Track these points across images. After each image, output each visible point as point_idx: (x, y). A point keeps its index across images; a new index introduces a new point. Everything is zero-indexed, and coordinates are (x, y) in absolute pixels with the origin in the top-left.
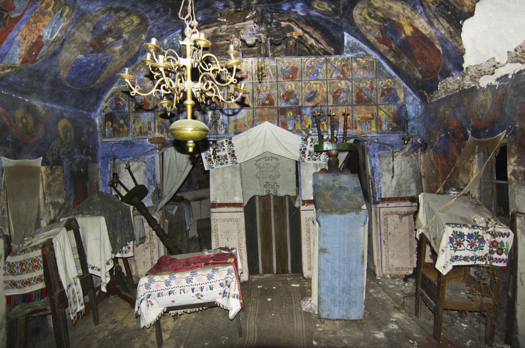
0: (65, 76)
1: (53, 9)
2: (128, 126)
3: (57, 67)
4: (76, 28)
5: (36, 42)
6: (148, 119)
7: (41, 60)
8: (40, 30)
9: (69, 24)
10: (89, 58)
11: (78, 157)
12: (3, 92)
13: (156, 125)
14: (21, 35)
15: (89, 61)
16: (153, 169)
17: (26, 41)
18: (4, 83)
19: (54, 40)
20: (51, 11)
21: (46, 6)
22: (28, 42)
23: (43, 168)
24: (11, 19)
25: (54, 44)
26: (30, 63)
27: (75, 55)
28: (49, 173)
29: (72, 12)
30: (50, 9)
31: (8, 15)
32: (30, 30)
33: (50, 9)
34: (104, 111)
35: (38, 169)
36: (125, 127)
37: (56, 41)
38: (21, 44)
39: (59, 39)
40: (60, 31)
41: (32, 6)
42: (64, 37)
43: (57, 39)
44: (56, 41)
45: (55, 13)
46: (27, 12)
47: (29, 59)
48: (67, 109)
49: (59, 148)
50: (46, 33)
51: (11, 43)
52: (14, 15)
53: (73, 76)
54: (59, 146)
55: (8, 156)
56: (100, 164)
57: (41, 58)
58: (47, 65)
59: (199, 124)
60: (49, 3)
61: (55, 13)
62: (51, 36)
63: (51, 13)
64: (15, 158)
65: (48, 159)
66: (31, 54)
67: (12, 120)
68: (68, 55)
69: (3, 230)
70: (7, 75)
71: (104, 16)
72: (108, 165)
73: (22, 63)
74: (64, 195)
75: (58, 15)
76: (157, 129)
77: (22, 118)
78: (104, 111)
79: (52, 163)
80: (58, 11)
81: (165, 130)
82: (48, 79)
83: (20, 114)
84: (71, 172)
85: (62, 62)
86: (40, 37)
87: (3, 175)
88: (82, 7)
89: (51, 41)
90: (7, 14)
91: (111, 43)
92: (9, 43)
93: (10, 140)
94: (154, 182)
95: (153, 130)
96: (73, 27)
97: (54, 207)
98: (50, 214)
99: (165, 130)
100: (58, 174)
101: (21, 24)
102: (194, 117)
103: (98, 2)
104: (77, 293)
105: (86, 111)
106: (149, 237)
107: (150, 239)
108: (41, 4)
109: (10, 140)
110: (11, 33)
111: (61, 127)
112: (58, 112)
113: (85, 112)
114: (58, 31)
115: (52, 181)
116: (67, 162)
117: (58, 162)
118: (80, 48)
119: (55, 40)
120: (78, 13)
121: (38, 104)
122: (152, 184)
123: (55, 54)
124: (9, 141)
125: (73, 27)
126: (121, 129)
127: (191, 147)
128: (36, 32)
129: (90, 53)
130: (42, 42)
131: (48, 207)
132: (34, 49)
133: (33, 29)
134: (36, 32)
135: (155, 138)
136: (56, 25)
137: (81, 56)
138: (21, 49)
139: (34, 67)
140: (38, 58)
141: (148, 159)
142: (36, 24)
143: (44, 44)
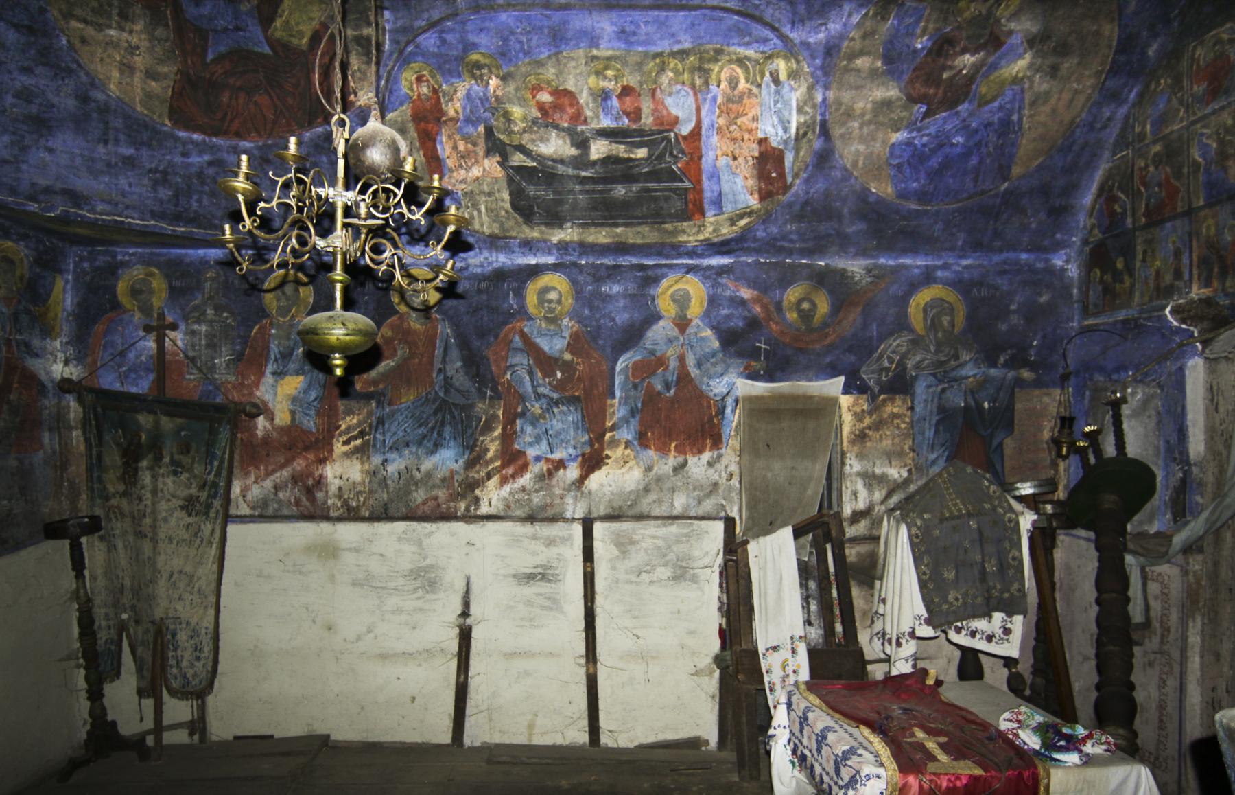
0: (889, 190)
1: (747, 81)
2: (1131, 275)
3: (852, 181)
4: (834, 85)
5: (761, 153)
6: (1174, 243)
7: (798, 181)
8: (752, 130)
9: (810, 89)
10: (932, 130)
11: (972, 373)
12: (762, 260)
13: (1195, 258)
14: (723, 155)
15: (937, 136)
16: (1179, 409)
17: (741, 160)
18: (752, 245)
19: (797, 133)
20: (748, 86)
21: (730, 84)
22: (747, 162)
23: (846, 401)
24: (685, 138)
25: (805, 140)
26: (778, 193)
27: (880, 140)
28: (863, 411)
29: (798, 62)
30: (743, 85)
31: (676, 135)
32: (734, 140)
33: (743, 85)
34: (1087, 240)
35: (833, 403)
36: (1126, 277)
37: (805, 134)
38: (734, 170)
39: (808, 127)
40: (800, 110)
41: (705, 100)
42: (819, 118)
43: (805, 129)
44: (805, 134)
45: (759, 86)
46: (703, 113)
47: (771, 188)
48: (951, 261)
49: (904, 357)
50: (771, 130)
51: (715, 176)
52: (685, 130)
53: (915, 185)
54: (904, 349)
55: (753, 376)
56: (1070, 389)
57: (796, 176)
58: (820, 186)
59: (359, 320)
60: (731, 76)
61: (759, 86)
62: (785, 130)
63: (750, 90)
64: (771, 379)
65: (862, 380)
66: (769, 177)
67: (772, 308)
68: (862, 148)
69: (727, 508)
70: (747, 229)
71: (891, 22)
72: (1084, 394)
73: (762, 199)
74: (909, 461)
75: (768, 86)
76: (1195, 272)
77: (800, 301)
78: (1087, 240)
79: (876, 389)
80: (762, 78)
81: (1216, 270)
82: (845, 211)
83: (796, 294)
84: (942, 410)
85: (855, 164)
86: (763, 141)
87: (737, 411)
88: (811, 40)
89: (793, 137)
90: (672, 135)
91: (977, 68)
92: (712, 177)
93: (763, 346)
94: (1181, 453)
95: (1186, 277)
96: (827, 87)
97: (870, 485)
98: (856, 498)
99: (1216, 270)
100: (893, 413)
101: (708, 137)
102: (348, 305)
103: (841, 6)
104: (794, 672)
105: (1028, 251)
106: (1159, 631)
107: (1162, 642)
108: (718, 86)
109: (763, 346)
110: (704, 159)
111: (918, 305)
112: (916, 271)
113: (1024, 256)
114: (794, 112)
115: (869, 428)
116: (928, 387)
117: (899, 385)
118: (881, 118)
119: (801, 132)
120: (813, 57)
121: (855, 266)
122: (1175, 459)
123: (824, 159)
124: (760, 348)
125: (827, 87)
126: (1118, 286)
127: (337, 366)
128: (746, 136)
129: (923, 119)
130: (774, 149)
131: (852, 481)
132: (768, 167)
133: (737, 134)
134: (746, 136)
135: (1192, 301)
136: (779, 105)
137: (898, 137)
138: (741, 177)
139: (793, 199)
140: (789, 180)
141: (1170, 375)
142: (736, 124)
143: (781, 151)
